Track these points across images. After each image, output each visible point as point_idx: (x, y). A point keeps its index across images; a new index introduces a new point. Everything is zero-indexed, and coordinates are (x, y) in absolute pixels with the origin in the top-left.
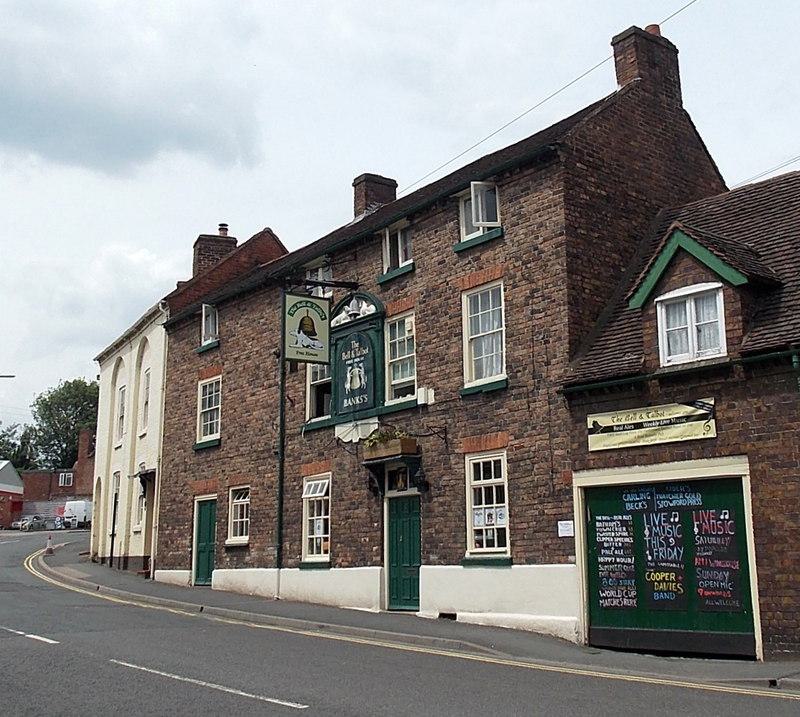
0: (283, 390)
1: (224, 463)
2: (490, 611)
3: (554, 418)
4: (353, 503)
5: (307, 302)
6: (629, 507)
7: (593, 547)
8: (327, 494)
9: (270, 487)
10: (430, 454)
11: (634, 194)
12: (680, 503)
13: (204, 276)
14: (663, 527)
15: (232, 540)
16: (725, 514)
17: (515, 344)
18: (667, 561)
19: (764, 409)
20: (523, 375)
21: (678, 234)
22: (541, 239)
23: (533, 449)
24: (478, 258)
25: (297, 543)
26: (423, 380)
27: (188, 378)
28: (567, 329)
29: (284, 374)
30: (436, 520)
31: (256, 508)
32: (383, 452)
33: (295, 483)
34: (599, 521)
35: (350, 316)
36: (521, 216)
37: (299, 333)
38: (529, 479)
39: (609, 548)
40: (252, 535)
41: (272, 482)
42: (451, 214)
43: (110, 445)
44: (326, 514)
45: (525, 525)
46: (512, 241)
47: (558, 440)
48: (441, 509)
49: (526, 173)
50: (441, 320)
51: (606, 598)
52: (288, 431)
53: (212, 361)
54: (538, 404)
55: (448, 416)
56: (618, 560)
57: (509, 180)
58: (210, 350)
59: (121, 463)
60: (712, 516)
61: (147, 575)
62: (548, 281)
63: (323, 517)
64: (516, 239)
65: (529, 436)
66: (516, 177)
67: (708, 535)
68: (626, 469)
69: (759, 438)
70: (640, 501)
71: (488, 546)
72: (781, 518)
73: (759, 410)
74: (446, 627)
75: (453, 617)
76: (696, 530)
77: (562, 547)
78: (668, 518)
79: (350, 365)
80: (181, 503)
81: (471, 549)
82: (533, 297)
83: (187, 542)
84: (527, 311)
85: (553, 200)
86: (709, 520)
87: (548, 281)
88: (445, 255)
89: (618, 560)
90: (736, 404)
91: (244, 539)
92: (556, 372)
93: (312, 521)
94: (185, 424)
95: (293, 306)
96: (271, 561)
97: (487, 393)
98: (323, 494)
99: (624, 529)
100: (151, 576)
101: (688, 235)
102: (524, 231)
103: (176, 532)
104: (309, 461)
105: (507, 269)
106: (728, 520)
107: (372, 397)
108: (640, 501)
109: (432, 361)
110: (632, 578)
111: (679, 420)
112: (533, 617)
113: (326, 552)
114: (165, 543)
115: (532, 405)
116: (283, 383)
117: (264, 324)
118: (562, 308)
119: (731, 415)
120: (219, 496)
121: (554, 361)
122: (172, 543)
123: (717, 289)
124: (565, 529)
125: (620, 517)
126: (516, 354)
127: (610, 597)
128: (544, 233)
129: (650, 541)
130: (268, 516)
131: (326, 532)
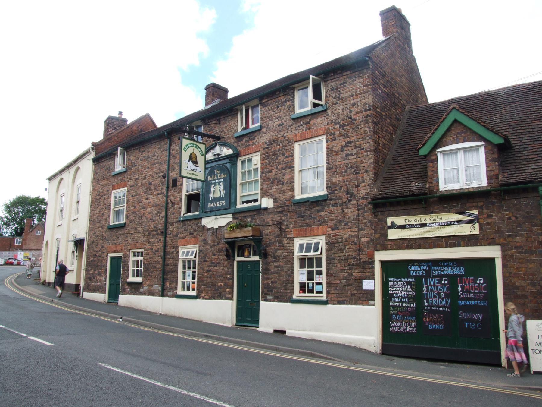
0: (167, 197)
1: (127, 237)
2: (310, 330)
3: (361, 218)
4: (213, 263)
5: (194, 144)
6: (413, 273)
7: (387, 297)
8: (195, 257)
9: (157, 251)
10: (269, 237)
11: (397, 95)
12: (449, 272)
13: (114, 135)
14: (437, 286)
15: (131, 279)
16: (481, 280)
17: (334, 174)
18: (438, 306)
19: (513, 218)
20: (339, 192)
21: (454, 112)
22: (354, 113)
23: (345, 236)
24: (308, 123)
25: (174, 284)
26: (264, 194)
27: (105, 189)
28: (372, 166)
29: (168, 188)
30: (272, 276)
31: (147, 263)
32: (239, 234)
33: (173, 250)
34: (391, 281)
35: (215, 155)
36: (339, 99)
37: (189, 161)
38: (342, 254)
39: (398, 297)
40: (145, 277)
41: (159, 248)
42: (289, 97)
43: (54, 224)
44: (194, 268)
45: (338, 282)
46: (333, 113)
47: (365, 232)
48: (276, 269)
49: (345, 74)
50: (279, 158)
51: (395, 326)
52: (169, 220)
53: (121, 180)
54: (349, 210)
55: (282, 215)
56: (404, 305)
57: (332, 78)
58: (120, 174)
59: (60, 234)
60: (471, 281)
61: (79, 295)
62: (358, 137)
63: (192, 270)
64: (336, 112)
65: (343, 229)
66: (338, 76)
67: (468, 292)
68: (414, 250)
69: (510, 236)
70: (421, 270)
71: (308, 292)
72: (523, 284)
73: (509, 219)
74: (279, 338)
75: (284, 332)
76: (460, 289)
77: (365, 295)
78: (440, 282)
79: (213, 184)
80: (100, 257)
81: (297, 294)
82: (347, 146)
83: (103, 279)
84: (343, 154)
85: (363, 90)
86: (469, 284)
87: (358, 137)
88: (283, 121)
89: (404, 305)
90: (493, 214)
91: (139, 279)
92: (363, 191)
93: (184, 273)
94: (103, 214)
95: (186, 146)
96: (157, 292)
97: (312, 202)
98: (193, 257)
99: (409, 286)
100: (81, 295)
101: (463, 113)
102: (342, 107)
103: (96, 272)
104: (184, 238)
105: (329, 129)
106: (482, 284)
107: (228, 202)
108: (421, 270)
109: (272, 183)
110: (413, 316)
111: (453, 223)
112: (356, 337)
113: (193, 290)
114: (89, 278)
115: (346, 211)
116: (167, 193)
117: (156, 160)
118: (369, 153)
119: (489, 221)
120: (123, 255)
121: (362, 185)
122: (94, 278)
123: (481, 146)
124: (367, 285)
125: (406, 279)
126: (334, 180)
127: (397, 326)
128: (356, 109)
129: (427, 294)
130: (155, 267)
131: (194, 278)
